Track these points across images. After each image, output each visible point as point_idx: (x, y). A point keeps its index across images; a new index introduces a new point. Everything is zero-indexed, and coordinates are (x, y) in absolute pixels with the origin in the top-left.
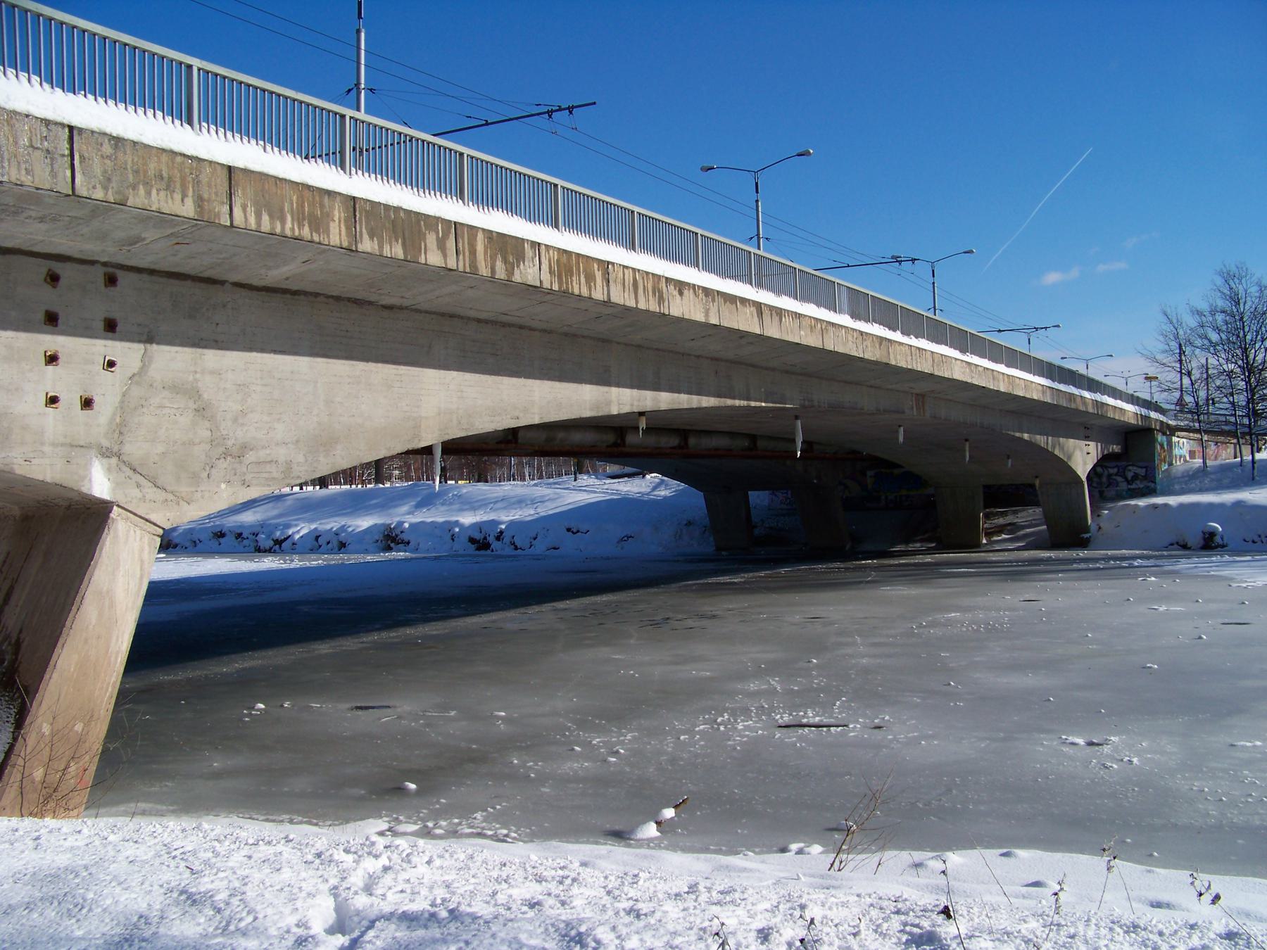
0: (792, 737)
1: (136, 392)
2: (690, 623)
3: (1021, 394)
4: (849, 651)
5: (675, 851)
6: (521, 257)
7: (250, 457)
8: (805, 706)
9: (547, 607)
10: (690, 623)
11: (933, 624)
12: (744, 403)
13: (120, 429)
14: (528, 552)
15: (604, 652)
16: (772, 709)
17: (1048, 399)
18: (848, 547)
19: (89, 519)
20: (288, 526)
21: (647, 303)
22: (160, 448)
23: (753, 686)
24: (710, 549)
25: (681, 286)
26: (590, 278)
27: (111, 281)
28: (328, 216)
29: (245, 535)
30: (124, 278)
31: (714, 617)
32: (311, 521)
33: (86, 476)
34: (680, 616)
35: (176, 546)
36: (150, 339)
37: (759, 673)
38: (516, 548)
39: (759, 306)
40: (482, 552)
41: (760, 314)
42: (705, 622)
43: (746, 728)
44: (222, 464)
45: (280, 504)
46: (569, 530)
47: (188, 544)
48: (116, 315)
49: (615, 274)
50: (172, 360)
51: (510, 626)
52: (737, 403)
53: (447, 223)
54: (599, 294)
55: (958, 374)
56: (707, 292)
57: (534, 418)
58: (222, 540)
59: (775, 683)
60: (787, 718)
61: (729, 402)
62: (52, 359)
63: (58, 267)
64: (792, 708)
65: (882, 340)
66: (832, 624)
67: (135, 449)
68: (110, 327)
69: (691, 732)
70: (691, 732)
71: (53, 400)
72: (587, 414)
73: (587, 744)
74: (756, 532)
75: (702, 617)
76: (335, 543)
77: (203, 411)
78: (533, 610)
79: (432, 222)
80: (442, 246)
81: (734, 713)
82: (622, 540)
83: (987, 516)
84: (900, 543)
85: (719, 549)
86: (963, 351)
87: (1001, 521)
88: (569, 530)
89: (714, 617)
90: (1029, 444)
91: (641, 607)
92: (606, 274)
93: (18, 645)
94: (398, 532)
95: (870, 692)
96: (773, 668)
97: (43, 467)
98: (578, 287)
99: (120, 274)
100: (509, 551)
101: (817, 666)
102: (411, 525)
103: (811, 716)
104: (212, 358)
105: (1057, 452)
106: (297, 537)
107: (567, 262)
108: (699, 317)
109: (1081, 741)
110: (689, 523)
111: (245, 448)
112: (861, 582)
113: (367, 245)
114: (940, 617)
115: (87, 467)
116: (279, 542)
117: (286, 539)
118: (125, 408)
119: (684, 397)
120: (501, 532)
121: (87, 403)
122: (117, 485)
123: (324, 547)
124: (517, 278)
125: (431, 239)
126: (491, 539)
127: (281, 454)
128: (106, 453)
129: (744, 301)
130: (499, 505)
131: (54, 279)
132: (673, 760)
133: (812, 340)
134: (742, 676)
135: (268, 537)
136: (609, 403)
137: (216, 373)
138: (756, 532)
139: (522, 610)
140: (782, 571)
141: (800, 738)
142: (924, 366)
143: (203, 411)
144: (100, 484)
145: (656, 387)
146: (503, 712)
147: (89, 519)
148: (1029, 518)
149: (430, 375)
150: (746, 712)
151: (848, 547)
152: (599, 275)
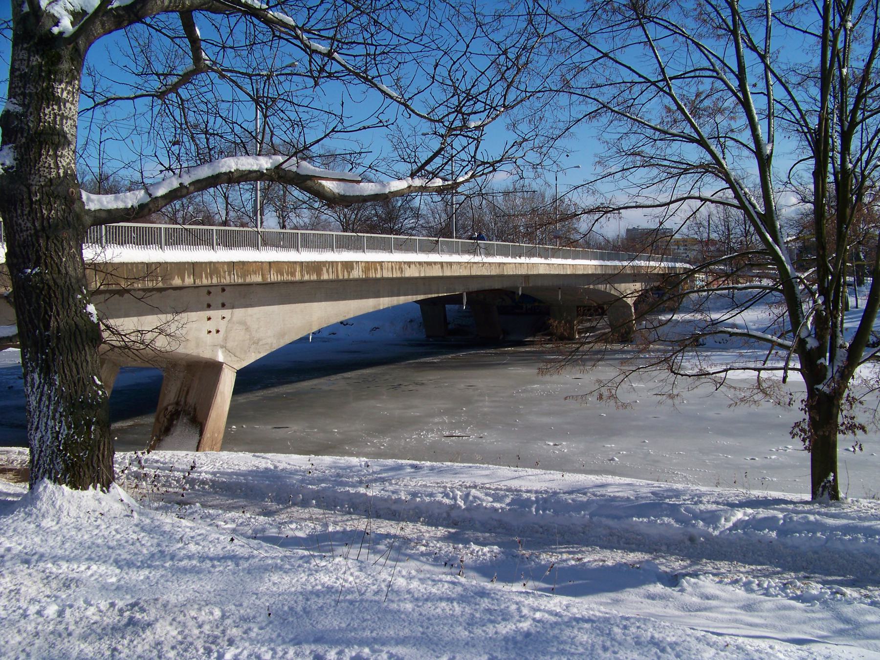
0: (448, 440)
1: (230, 325)
2: (411, 387)
3: (581, 273)
4: (481, 404)
6: (352, 268)
7: (260, 343)
8: (455, 429)
9: (339, 376)
10: (411, 387)
11: (524, 391)
12: (436, 295)
13: (226, 339)
15: (372, 403)
16: (443, 430)
17: (599, 272)
18: (501, 337)
19: (215, 368)
21: (397, 274)
22: (236, 343)
23: (436, 420)
24: (422, 336)
25: (409, 264)
26: (376, 270)
27: (223, 290)
28: (295, 271)
30: (227, 289)
31: (423, 384)
33: (217, 355)
34: (406, 384)
36: (233, 308)
37: (441, 414)
39: (441, 263)
41: (442, 267)
42: (418, 387)
43: (432, 437)
44: (253, 346)
48: (225, 301)
49: (385, 266)
50: (239, 313)
51: (325, 388)
52: (433, 296)
53: (329, 262)
54: (379, 276)
55: (542, 271)
56: (420, 263)
57: (351, 315)
59: (446, 419)
60: (447, 433)
61: (430, 296)
62: (209, 319)
63: (209, 289)
64: (451, 429)
65: (500, 264)
66: (477, 389)
67: (229, 345)
68: (223, 305)
69: (411, 438)
70: (411, 438)
71: (210, 332)
72: (371, 310)
73: (372, 442)
74: (450, 327)
75: (417, 384)
77: (247, 329)
78: (333, 378)
79: (324, 263)
80: (328, 271)
81: (427, 431)
82: (372, 330)
83: (581, 322)
84: (530, 336)
85: (428, 337)
86: (546, 258)
87: (588, 325)
89: (423, 384)
90: (594, 289)
91: (387, 377)
92: (382, 266)
93: (195, 409)
95: (483, 424)
96: (446, 412)
97: (206, 354)
98: (372, 275)
99: (226, 288)
101: (465, 412)
103: (457, 433)
104: (250, 310)
105: (613, 292)
107: (368, 265)
108: (417, 275)
109: (552, 444)
110: (411, 321)
111: (259, 340)
112: (499, 364)
113: (306, 278)
114: (529, 387)
115: (217, 352)
118: (227, 331)
119: (410, 297)
121: (218, 331)
122: (225, 357)
124: (351, 277)
125: (325, 270)
127: (269, 341)
128: (222, 347)
129: (435, 263)
131: (209, 293)
132: (404, 448)
133: (464, 272)
134: (432, 416)
136: (379, 305)
137: (251, 316)
138: (450, 327)
139: (327, 378)
140: (461, 354)
141: (451, 441)
142: (523, 271)
143: (247, 329)
144: (221, 358)
145: (398, 295)
147: (215, 368)
148: (602, 324)
149: (315, 305)
150: (432, 431)
151: (501, 337)
152: (379, 268)
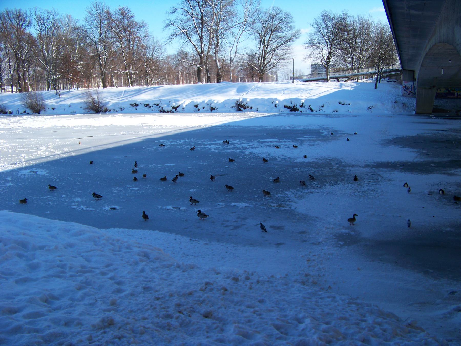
5: (395, 162)
14: (319, 112)
20: (178, 101)
29: (151, 105)
32: (189, 97)
35: (110, 111)
38: (312, 111)
40: (293, 112)
45: (156, 91)
46: (340, 103)
47: (117, 110)
58: (137, 108)
76: (207, 108)
88: (340, 103)
94: (244, 103)
100: (309, 112)
102: (251, 100)
106: (184, 106)
116: (175, 108)
117: (178, 107)
120: (303, 104)
123: (201, 109)
126: (298, 107)
130: (286, 92)
135: (168, 106)
146: (454, 134)
